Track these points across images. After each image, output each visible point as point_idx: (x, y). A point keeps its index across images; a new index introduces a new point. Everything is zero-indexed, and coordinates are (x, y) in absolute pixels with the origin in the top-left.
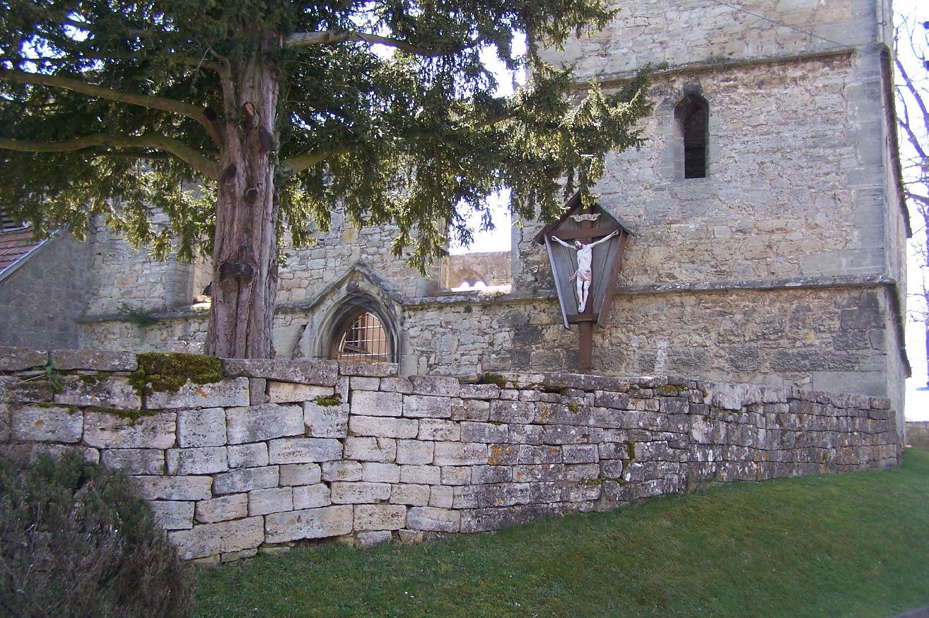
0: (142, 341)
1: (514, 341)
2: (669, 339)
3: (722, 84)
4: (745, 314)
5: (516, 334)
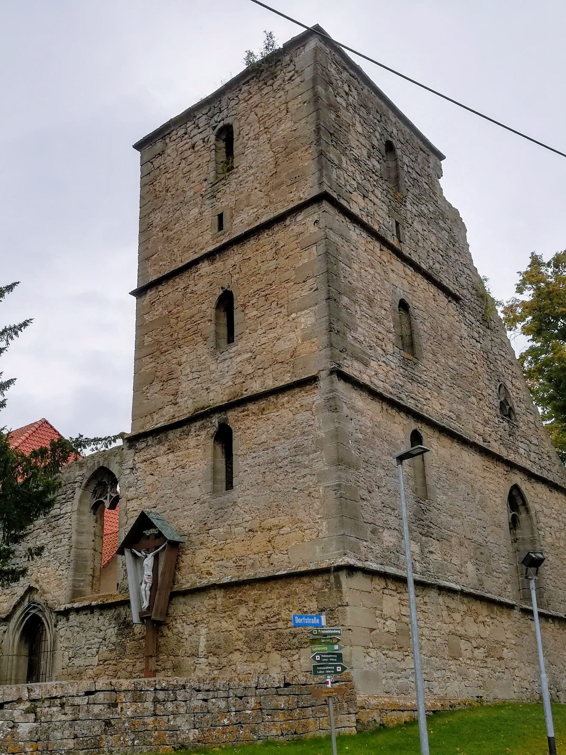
4: (254, 601)
5: (118, 630)
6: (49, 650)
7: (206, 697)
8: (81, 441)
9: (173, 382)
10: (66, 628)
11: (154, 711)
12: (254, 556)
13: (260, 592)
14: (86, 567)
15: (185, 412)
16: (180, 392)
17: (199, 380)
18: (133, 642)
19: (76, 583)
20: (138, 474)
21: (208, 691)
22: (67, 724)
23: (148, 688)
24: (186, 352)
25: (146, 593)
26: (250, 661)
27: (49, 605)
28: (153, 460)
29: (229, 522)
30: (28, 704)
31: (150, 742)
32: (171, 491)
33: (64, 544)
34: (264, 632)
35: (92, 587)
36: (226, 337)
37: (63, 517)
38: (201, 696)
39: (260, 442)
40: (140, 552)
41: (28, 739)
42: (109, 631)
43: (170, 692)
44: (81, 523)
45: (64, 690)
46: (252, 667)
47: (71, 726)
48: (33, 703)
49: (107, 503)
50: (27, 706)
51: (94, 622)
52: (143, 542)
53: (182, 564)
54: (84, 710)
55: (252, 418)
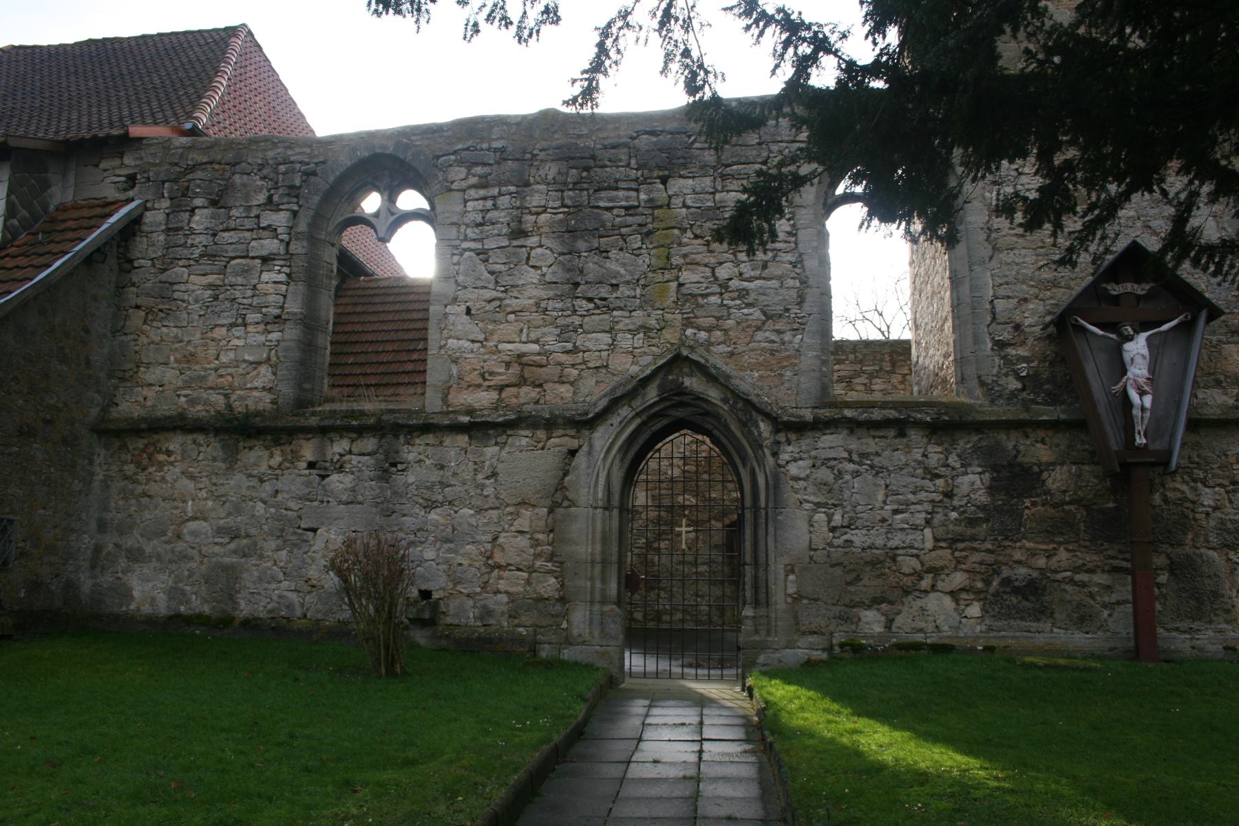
0: (231, 468)
1: (991, 490)
5: (992, 479)
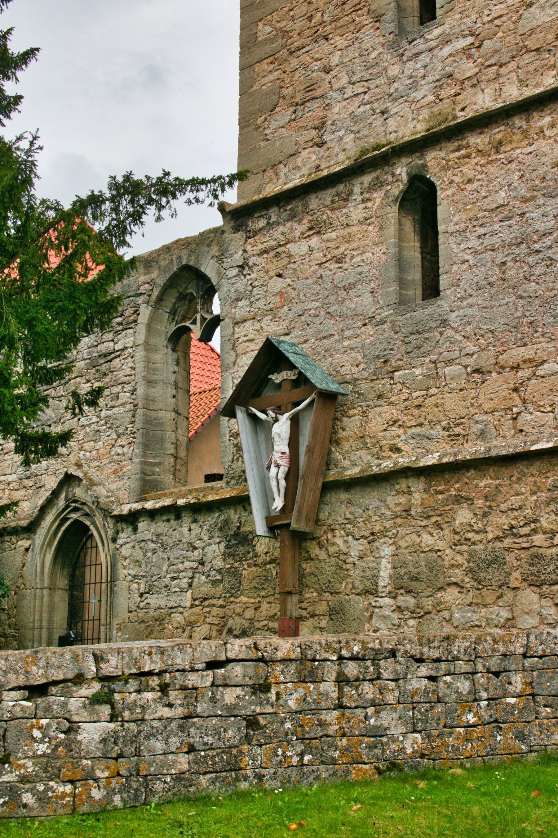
1: (225, 556)
2: (394, 543)
3: (451, 156)
4: (486, 498)
5: (227, 547)
6: (104, 580)
7: (434, 673)
8: (168, 184)
9: (315, 104)
10: (132, 544)
11: (339, 699)
12: (484, 417)
13: (497, 482)
14: (163, 440)
15: (341, 157)
16: (329, 122)
17: (367, 97)
18: (254, 569)
19: (147, 467)
20: (253, 276)
21: (438, 660)
22: (174, 725)
23: (327, 655)
24: (339, 47)
25: (278, 482)
26: (477, 604)
27: (102, 505)
28: (280, 250)
29: (434, 357)
30: (96, 687)
31: (333, 759)
32: (318, 304)
33: (122, 401)
34: (506, 553)
35: (174, 475)
36: (417, 13)
37: (119, 356)
38: (424, 670)
39: (494, 206)
40: (264, 412)
41: (99, 754)
42: (209, 549)
43: (369, 663)
44: (151, 365)
45: (165, 658)
46: (483, 614)
47: (182, 728)
48: (106, 684)
49: (196, 331)
50: (94, 691)
51: (181, 534)
52: (268, 393)
53: (342, 434)
54: (206, 698)
55: (475, 161)
